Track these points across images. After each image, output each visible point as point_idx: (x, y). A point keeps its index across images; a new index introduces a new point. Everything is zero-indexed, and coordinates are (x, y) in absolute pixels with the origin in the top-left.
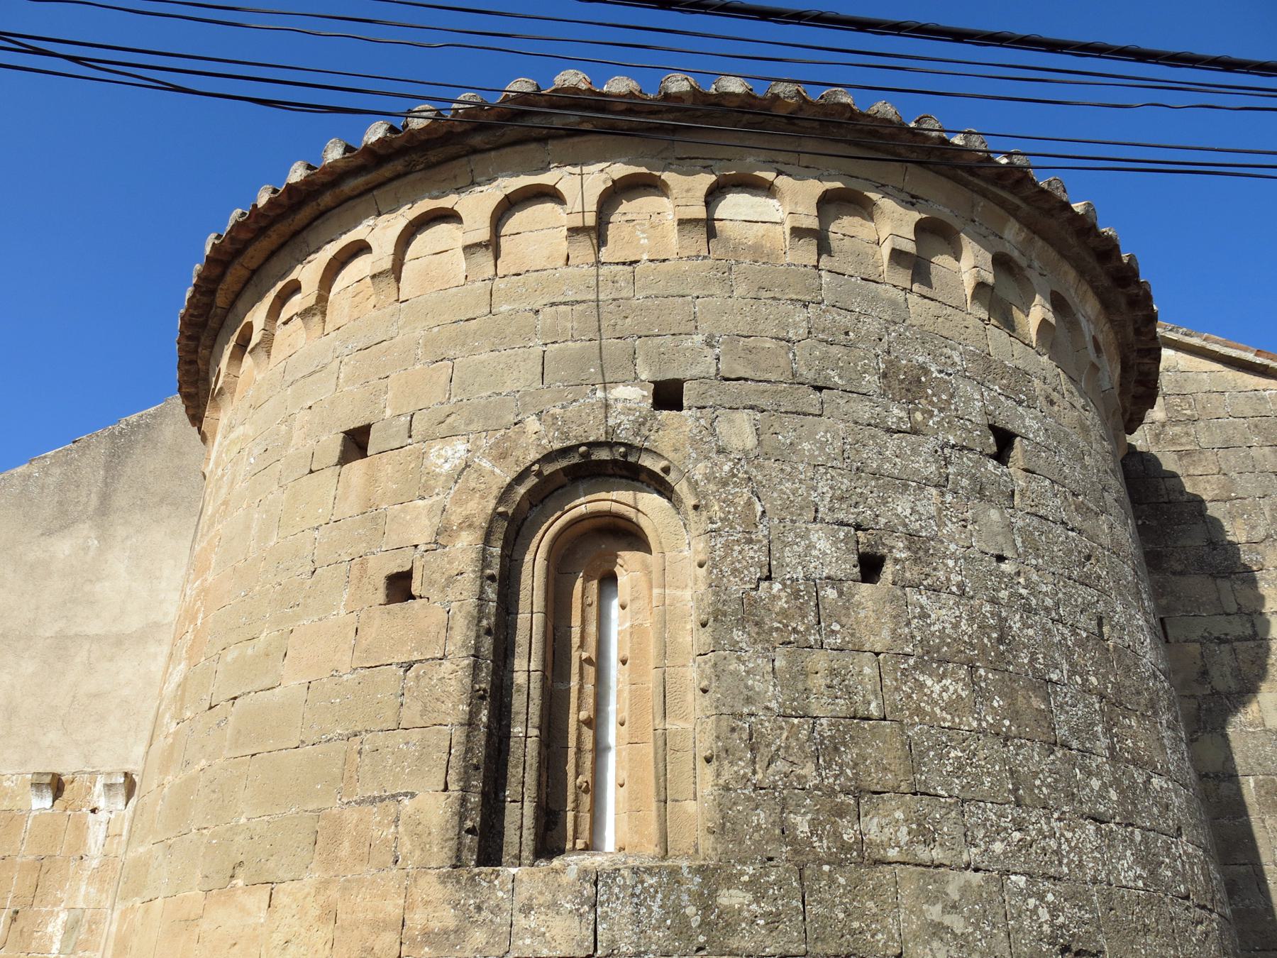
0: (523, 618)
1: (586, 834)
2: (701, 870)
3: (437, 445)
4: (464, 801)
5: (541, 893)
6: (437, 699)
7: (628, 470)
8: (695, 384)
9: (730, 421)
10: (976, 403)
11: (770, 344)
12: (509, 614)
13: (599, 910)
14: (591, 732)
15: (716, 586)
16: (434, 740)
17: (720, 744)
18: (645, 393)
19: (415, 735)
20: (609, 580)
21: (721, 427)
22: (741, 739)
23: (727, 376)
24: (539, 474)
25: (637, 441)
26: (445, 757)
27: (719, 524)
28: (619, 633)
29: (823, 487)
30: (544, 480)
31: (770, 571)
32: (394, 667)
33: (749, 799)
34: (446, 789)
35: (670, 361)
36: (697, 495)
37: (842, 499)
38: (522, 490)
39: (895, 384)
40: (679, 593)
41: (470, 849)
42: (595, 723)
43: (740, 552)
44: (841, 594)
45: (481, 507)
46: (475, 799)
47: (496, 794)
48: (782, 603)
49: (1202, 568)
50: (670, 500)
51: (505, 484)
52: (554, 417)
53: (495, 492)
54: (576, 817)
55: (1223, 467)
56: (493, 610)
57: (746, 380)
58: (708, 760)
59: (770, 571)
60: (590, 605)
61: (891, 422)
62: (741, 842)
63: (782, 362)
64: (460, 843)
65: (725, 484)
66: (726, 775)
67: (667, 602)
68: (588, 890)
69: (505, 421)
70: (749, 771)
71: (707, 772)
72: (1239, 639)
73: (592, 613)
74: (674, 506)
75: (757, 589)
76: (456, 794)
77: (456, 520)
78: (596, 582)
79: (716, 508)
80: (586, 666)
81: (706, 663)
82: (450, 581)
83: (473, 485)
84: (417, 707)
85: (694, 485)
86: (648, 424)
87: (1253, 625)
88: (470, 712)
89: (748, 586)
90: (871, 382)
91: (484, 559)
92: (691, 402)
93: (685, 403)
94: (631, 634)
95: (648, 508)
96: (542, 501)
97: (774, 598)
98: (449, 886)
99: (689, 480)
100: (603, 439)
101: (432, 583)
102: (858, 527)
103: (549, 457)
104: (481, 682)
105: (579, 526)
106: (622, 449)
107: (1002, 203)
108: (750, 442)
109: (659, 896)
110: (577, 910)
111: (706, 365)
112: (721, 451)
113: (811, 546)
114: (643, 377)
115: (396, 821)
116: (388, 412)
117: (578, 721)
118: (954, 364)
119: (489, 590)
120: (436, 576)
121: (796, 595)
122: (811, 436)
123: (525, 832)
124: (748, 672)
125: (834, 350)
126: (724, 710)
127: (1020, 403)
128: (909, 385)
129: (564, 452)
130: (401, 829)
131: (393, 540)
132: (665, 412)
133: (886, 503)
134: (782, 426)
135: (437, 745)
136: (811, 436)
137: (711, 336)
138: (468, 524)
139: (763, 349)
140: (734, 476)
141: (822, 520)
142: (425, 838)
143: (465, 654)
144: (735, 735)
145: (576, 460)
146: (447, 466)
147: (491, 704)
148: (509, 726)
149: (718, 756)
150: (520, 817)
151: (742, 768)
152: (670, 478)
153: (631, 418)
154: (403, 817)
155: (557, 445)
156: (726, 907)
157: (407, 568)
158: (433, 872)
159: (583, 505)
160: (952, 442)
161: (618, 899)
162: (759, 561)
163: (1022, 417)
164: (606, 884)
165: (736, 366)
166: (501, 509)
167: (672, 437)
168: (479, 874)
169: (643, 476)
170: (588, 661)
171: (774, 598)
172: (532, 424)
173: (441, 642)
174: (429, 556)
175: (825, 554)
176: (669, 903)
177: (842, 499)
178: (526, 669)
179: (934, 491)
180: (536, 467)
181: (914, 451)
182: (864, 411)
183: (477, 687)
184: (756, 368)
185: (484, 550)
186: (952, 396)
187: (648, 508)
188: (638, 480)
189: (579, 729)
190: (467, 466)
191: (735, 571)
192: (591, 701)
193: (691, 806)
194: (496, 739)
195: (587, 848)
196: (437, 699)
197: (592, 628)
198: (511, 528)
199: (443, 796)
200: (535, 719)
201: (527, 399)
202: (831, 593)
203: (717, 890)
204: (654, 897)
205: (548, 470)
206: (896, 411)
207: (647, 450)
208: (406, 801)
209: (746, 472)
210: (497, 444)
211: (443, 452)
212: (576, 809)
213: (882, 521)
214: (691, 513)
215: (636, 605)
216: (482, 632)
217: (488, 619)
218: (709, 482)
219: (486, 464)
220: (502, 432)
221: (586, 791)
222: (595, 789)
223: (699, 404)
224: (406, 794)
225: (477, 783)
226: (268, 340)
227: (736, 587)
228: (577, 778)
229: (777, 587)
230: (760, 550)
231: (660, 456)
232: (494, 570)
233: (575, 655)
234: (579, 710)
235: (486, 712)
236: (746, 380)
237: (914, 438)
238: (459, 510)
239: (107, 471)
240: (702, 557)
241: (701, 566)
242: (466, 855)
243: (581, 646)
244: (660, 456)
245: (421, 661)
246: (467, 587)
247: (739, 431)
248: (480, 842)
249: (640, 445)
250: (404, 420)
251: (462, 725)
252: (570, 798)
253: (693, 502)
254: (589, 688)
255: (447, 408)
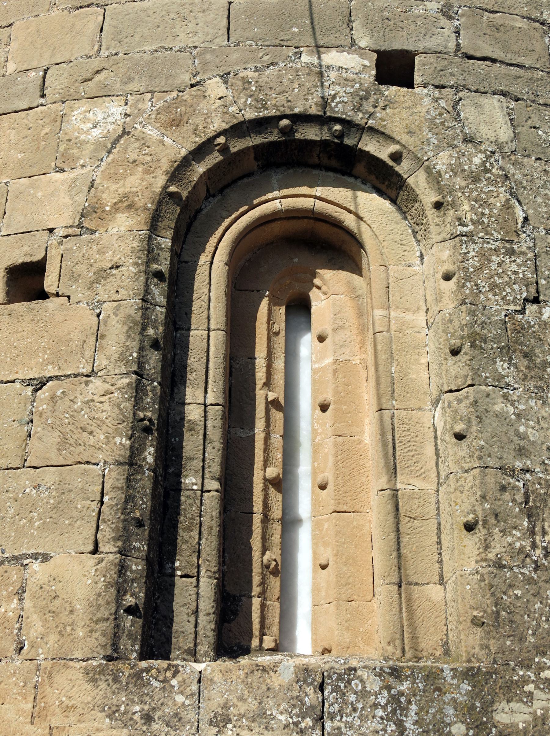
0: (196, 335)
1: (275, 629)
2: (469, 674)
3: (82, 107)
4: (122, 568)
5: (242, 699)
6: (83, 429)
7: (341, 155)
8: (431, 58)
9: (478, 106)
11: (520, 23)
12: (177, 329)
13: (328, 725)
14: (279, 497)
15: (470, 303)
16: (78, 482)
17: (487, 506)
18: (367, 63)
19: (50, 476)
20: (299, 308)
21: (467, 112)
22: (514, 500)
23: (471, 52)
24: (224, 149)
25: (359, 118)
26: (95, 506)
27: (471, 227)
28: (315, 372)
30: (231, 160)
31: (538, 292)
32: (17, 385)
33: (529, 581)
34: (95, 550)
35: (398, 28)
36: (440, 190)
38: (200, 169)
40: (409, 317)
41: (130, 636)
42: (283, 484)
43: (500, 264)
45: (147, 184)
46: (137, 566)
47: (161, 566)
50: (394, 201)
51: (179, 157)
52: (246, 81)
53: (165, 165)
54: (263, 606)
56: (162, 318)
57: (494, 61)
58: (469, 527)
59: (538, 292)
60: (277, 334)
62: (522, 639)
64: (117, 626)
65: (476, 180)
66: (498, 547)
67: (393, 328)
68: (311, 697)
69: (178, 82)
70: (527, 544)
71: (471, 544)
73: (280, 342)
74: (400, 209)
75: (522, 312)
76: (111, 557)
77: (109, 199)
78: (283, 310)
79: (466, 207)
80: (273, 411)
81: (459, 401)
82: (102, 275)
83: (133, 156)
84: (54, 438)
85: (435, 178)
86: (372, 100)
88: (132, 447)
89: (512, 307)
91: (150, 251)
92: (426, 79)
93: (418, 79)
94: (335, 371)
95: (367, 211)
96: (221, 191)
98: (103, 685)
99: (428, 170)
100: (314, 110)
101: (74, 277)
103: (238, 129)
104: (144, 409)
105: (267, 229)
106: (338, 127)
108: (505, 134)
109: (414, 707)
110: (296, 724)
111: (444, 37)
112: (468, 140)
114: (363, 44)
115: (21, 593)
116: (11, 67)
117: (265, 479)
119: (156, 292)
120: (81, 269)
123: (202, 619)
124: (518, 416)
126: (491, 462)
129: (260, 125)
130: (28, 604)
131: (17, 220)
132: (394, 88)
134: (542, 119)
135: (83, 490)
138: (126, 204)
139: (513, 28)
140: (487, 171)
142: (64, 617)
143: (123, 370)
144: (507, 496)
145: (274, 136)
146: (96, 133)
147: (159, 439)
148: (178, 475)
149: (485, 522)
150: (195, 597)
151: (518, 539)
152: (402, 168)
153: (349, 90)
154: (31, 587)
155: (251, 115)
156: (506, 726)
157: (38, 257)
158: (78, 665)
159: (277, 200)
161: (355, 710)
162: (524, 278)
164: (336, 689)
165: (480, 43)
166: (173, 189)
167: (404, 119)
168: (147, 670)
170: (275, 403)
172: (215, 88)
173: (89, 353)
174: (69, 243)
176: (428, 718)
178: (203, 400)
180: (221, 140)
183: (141, 415)
184: (506, 48)
185: (150, 238)
188: (350, 175)
189: (265, 490)
190: (125, 133)
191: (494, 287)
192: (279, 456)
193: (435, 592)
194: (161, 490)
195: (275, 650)
196: (83, 429)
197: (279, 364)
198: (185, 215)
199: (92, 560)
200: (215, 468)
201: (208, 57)
203: (493, 702)
204: (407, 709)
205: (236, 146)
207: (372, 130)
208: (36, 566)
209: (501, 168)
210: (167, 108)
211: (91, 115)
212: (262, 594)
214: (431, 213)
215: (341, 336)
216: (147, 344)
217: (155, 327)
218: (455, 174)
219: (152, 132)
220: (174, 94)
221: (275, 572)
222: (283, 570)
223: (437, 82)
224: (35, 556)
225: (140, 545)
227: (497, 307)
228: (263, 554)
230: (524, 263)
231: (390, 138)
232: (164, 265)
233: (260, 394)
234: (266, 465)
235: (152, 450)
236: (494, 61)
238: (114, 187)
240: (449, 267)
241: (447, 277)
242: (125, 643)
243: (268, 384)
244: (390, 138)
245: (58, 378)
246: (127, 284)
248: (144, 626)
249: (363, 122)
250: (35, 76)
251: (120, 464)
252: (256, 579)
253: (435, 198)
254: (277, 439)
255: (96, 64)
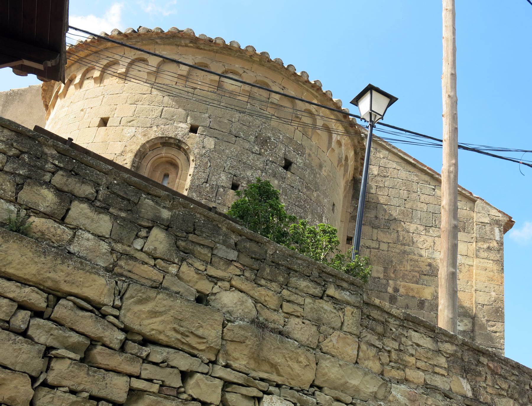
10: (281, 151)
11: (226, 121)
29: (228, 163)
37: (233, 167)
39: (259, 140)
44: (224, 191)
48: (208, 189)
49: (370, 224)
55: (389, 193)
61: (254, 150)
63: (228, 127)
65: (202, 156)
72: (373, 248)
77: (128, 149)
87: (379, 245)
90: (252, 138)
97: (206, 188)
100: (173, 137)
102: (235, 176)
107: (313, 94)
108: (213, 146)
113: (220, 177)
118: (279, 139)
121: (212, 188)
122: (229, 149)
125: (244, 127)
127: (298, 154)
128: (263, 142)
133: (244, 171)
134: (222, 144)
136: (229, 149)
137: (211, 115)
141: (225, 171)
152: (188, 151)
160: (271, 160)
163: (297, 158)
169: (182, 150)
171: (206, 188)
175: (223, 180)
177: (233, 167)
179: (260, 171)
181: (258, 160)
182: (247, 146)
186: (276, 147)
187: (180, 159)
202: (222, 190)
206: (256, 148)
213: (242, 175)
226: (81, 84)
227: (197, 183)
229: (208, 185)
237: (259, 156)
239: (3, 107)
247: (210, 143)
250: (120, 119)
255: (132, 119)
